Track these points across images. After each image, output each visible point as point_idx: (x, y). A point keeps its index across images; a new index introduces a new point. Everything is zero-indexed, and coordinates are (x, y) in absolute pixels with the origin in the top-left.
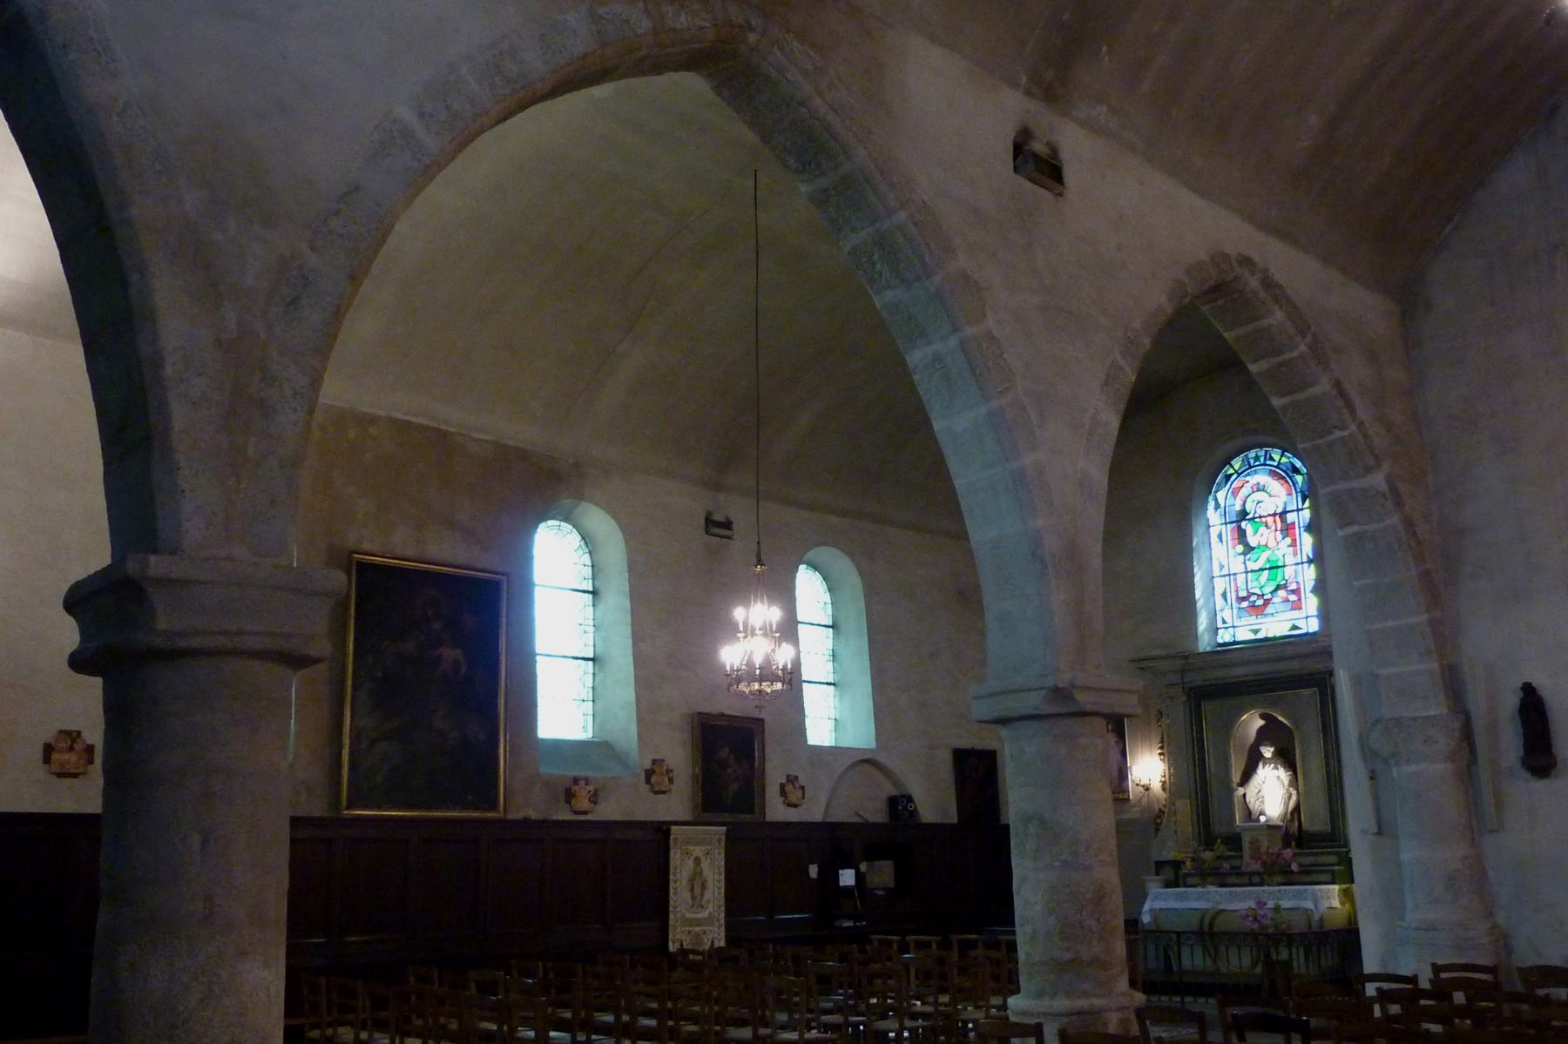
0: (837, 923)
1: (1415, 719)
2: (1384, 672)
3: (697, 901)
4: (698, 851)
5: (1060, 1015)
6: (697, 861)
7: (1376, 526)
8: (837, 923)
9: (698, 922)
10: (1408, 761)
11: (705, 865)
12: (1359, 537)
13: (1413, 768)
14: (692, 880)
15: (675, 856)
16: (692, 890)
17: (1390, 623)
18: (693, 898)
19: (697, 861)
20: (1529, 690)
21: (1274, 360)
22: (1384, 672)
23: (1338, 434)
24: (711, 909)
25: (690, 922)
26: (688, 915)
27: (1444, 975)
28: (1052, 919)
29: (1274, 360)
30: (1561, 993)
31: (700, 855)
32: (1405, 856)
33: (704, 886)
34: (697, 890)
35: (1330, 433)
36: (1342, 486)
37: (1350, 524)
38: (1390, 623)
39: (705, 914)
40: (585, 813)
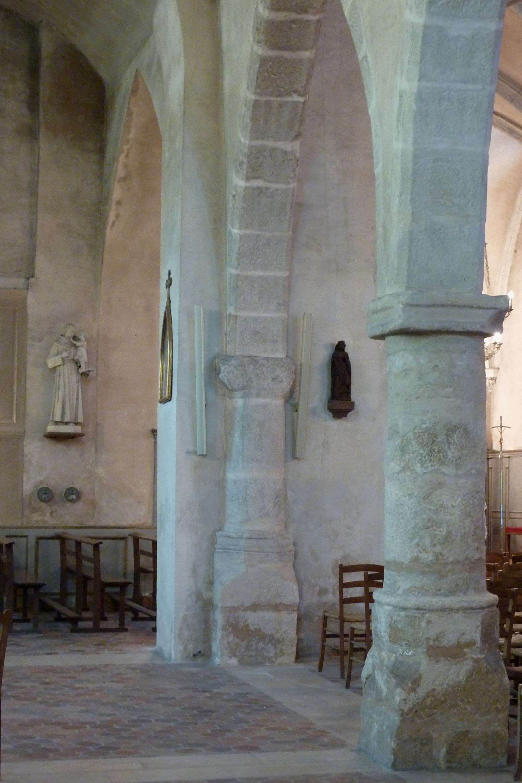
1: (268, 359)
2: (241, 314)
5: (482, 608)
7: (280, 186)
10: (258, 395)
12: (260, 191)
13: (260, 401)
17: (259, 273)
20: (340, 347)
21: (293, 16)
22: (241, 314)
23: (296, 98)
27: (107, 590)
28: (468, 522)
29: (293, 16)
32: (231, 476)
35: (290, 94)
36: (270, 143)
37: (258, 178)
38: (259, 273)
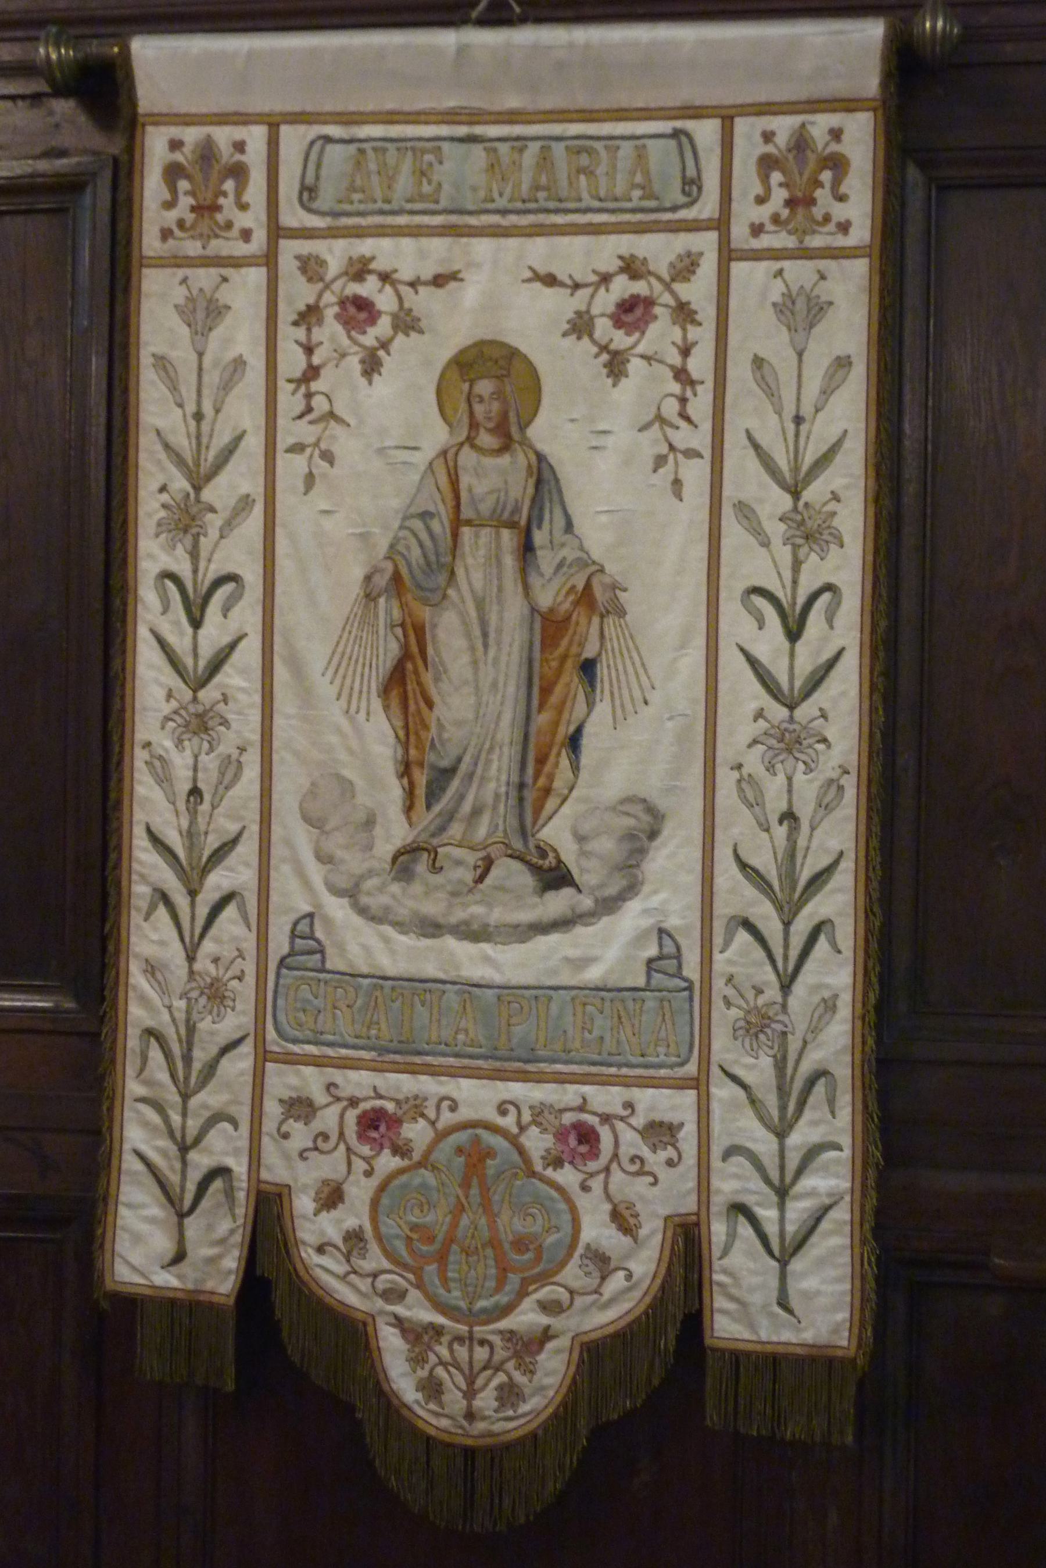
0: (928, 18)
3: (492, 808)
4: (501, 290)
6: (492, 387)
8: (928, 18)
9: (507, 1034)
11: (600, 443)
14: (407, 588)
15: (196, 345)
16: (405, 686)
18: (428, 776)
19: (492, 387)
24: (668, 891)
25: (403, 1022)
26: (365, 946)
30: (3, 208)
31: (532, 322)
33: (568, 649)
34: (477, 695)
39: (610, 949)
40: (674, 209)
